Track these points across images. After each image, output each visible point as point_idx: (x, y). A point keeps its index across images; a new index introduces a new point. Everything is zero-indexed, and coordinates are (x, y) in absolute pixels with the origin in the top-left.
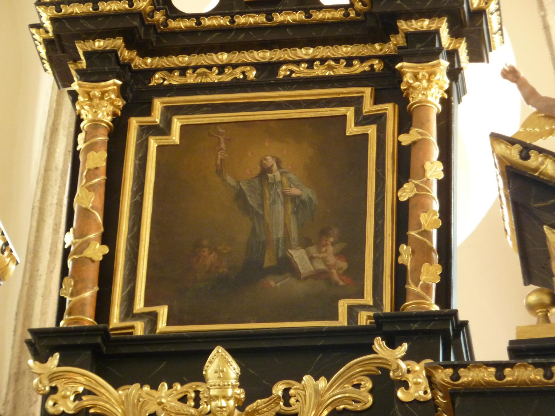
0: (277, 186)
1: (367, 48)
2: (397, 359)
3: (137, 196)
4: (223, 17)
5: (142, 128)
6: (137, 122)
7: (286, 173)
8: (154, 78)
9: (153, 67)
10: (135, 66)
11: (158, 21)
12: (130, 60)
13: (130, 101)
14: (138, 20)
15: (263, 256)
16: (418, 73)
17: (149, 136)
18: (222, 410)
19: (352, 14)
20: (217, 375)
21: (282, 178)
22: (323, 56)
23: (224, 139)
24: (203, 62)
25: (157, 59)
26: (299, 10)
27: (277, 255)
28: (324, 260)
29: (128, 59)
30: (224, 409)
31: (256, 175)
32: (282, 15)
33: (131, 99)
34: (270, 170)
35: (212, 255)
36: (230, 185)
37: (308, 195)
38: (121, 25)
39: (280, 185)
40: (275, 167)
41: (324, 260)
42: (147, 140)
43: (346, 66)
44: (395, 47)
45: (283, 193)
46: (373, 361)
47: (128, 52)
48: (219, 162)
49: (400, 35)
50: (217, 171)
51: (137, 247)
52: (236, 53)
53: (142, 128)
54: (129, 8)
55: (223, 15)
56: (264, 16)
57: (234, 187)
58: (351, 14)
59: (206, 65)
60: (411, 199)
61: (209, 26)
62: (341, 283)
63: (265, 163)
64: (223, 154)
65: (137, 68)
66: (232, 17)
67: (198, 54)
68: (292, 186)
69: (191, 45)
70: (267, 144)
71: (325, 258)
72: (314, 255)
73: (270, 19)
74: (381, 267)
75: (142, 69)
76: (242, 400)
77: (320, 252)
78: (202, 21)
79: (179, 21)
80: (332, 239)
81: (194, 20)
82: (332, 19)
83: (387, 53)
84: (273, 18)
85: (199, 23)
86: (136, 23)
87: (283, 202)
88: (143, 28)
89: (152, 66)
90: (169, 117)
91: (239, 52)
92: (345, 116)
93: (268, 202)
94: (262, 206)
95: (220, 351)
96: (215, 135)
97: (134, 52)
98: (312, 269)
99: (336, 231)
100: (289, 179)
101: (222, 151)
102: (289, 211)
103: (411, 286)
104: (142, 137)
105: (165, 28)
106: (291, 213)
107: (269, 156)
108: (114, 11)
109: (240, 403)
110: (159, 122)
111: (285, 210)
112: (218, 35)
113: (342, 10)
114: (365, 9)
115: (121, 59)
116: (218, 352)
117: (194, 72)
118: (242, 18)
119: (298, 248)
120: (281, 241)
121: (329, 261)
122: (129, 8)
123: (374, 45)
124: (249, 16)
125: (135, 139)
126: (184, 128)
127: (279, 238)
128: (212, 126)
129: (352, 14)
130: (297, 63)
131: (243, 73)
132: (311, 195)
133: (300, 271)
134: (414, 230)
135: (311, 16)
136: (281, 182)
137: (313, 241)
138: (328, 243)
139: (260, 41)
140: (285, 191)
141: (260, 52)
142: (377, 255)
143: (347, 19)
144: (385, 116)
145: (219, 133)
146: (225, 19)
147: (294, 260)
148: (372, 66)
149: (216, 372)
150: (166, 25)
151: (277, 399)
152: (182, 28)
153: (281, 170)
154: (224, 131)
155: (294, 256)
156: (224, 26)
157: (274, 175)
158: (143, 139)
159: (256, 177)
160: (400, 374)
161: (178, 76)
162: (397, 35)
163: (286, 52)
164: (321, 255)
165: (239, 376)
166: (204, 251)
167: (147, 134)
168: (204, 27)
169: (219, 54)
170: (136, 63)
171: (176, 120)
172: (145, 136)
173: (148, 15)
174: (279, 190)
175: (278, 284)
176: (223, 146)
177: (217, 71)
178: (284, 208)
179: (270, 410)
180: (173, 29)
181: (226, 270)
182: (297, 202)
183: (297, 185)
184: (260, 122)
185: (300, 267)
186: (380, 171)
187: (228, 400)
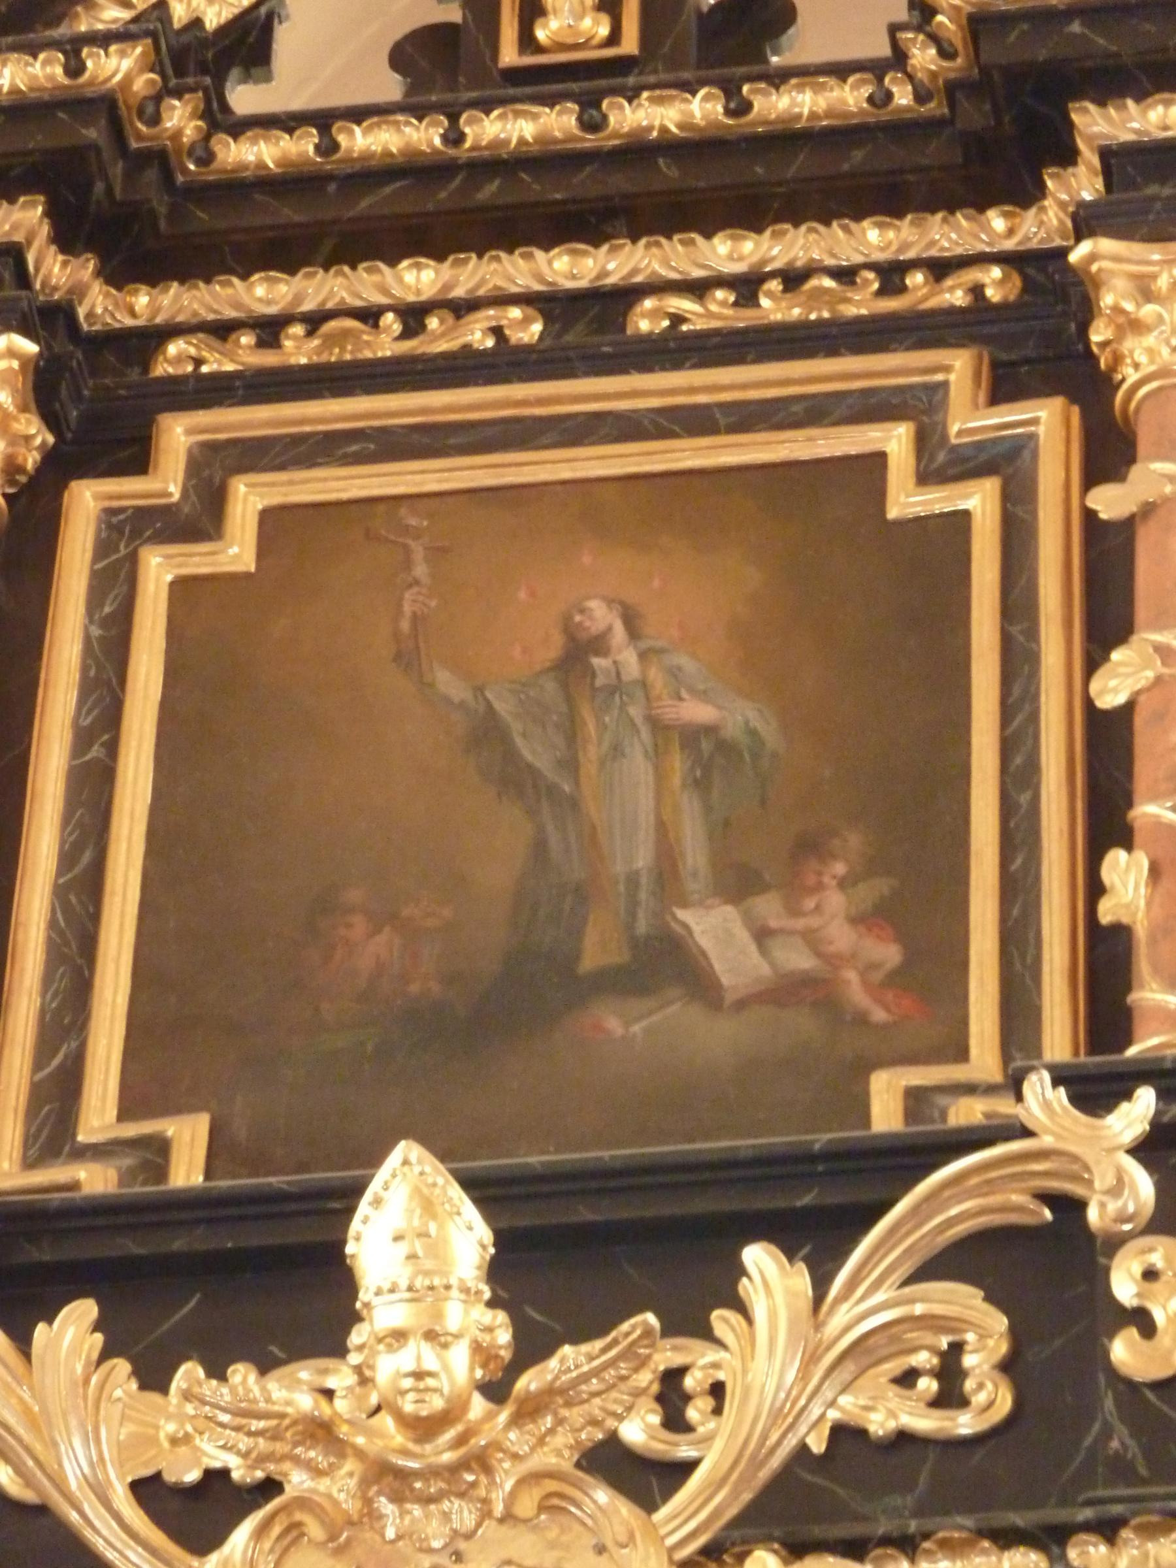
0: (628, 695)
1: (958, 228)
2: (1112, 1150)
3: (96, 747)
4: (420, 119)
5: (114, 520)
6: (97, 497)
7: (661, 651)
8: (161, 358)
9: (158, 320)
10: (90, 315)
11: (177, 134)
12: (70, 291)
13: (69, 435)
14: (103, 122)
15: (577, 933)
16: (1154, 277)
17: (141, 545)
18: (422, 1385)
19: (903, 97)
20: (403, 1248)
21: (644, 672)
22: (795, 259)
23: (425, 549)
24: (345, 295)
25: (172, 291)
26: (703, 83)
27: (630, 926)
28: (812, 939)
29: (65, 289)
30: (430, 1382)
31: (548, 664)
32: (640, 105)
33: (73, 425)
34: (599, 644)
35: (382, 938)
36: (447, 700)
37: (747, 723)
38: (37, 140)
39: (639, 693)
40: (619, 633)
41: (812, 939)
42: (133, 560)
43: (881, 292)
44: (1062, 215)
45: (657, 725)
46: (1018, 1168)
47: (65, 264)
48: (405, 625)
49: (1081, 169)
50: (398, 657)
51: (93, 917)
52: (469, 259)
53: (114, 520)
54: (66, 81)
55: (420, 113)
56: (571, 111)
57: (462, 705)
58: (896, 96)
59: (360, 308)
60: (1142, 699)
61: (367, 156)
62: (879, 1015)
63: (580, 623)
64: (421, 598)
65: (97, 327)
66: (454, 118)
67: (326, 269)
68: (684, 694)
69: (299, 225)
70: (587, 559)
71: (817, 930)
72: (773, 924)
73: (592, 125)
74: (1031, 951)
75: (116, 330)
76: (502, 1353)
77: (795, 912)
78: (342, 139)
79: (254, 141)
80: (840, 868)
81: (313, 136)
82: (829, 114)
83: (1034, 244)
84: (605, 117)
85: (328, 147)
86: (91, 134)
87: (650, 749)
88: (120, 164)
89: (154, 317)
90: (217, 480)
91: (480, 256)
92: (880, 458)
93: (591, 754)
94: (571, 765)
95: (413, 1157)
96: (392, 537)
97: (88, 260)
98: (765, 970)
99: (854, 840)
100: (674, 673)
101: (415, 589)
102: (676, 780)
103: (1152, 990)
104: (117, 550)
105: (203, 170)
106: (684, 786)
107: (595, 597)
108: (10, 92)
109: (492, 1366)
110: (176, 497)
111: (660, 777)
112: (401, 187)
113: (864, 82)
114: (949, 69)
115: (38, 286)
116: (406, 1162)
117: (310, 333)
118: (491, 122)
119: (709, 902)
120: (644, 880)
121: (831, 943)
122: (66, 81)
123: (983, 218)
124: (518, 114)
125: (89, 555)
126: (271, 519)
127: (637, 872)
128: (381, 508)
129: (903, 97)
130: (698, 289)
131: (497, 331)
132: (757, 723)
133: (718, 980)
134: (1155, 797)
135: (746, 107)
136: (644, 684)
137: (767, 877)
138: (826, 879)
139: (556, 203)
140: (659, 711)
141: (560, 255)
142: (1015, 912)
143: (884, 115)
144: (1032, 445)
145: (406, 530)
146: (427, 128)
147: (696, 943)
148: (977, 291)
149: (398, 1238)
150: (207, 158)
151: (640, 1337)
152: (266, 167)
153: (644, 645)
154: (425, 523)
155: (697, 929)
156: (423, 153)
157: (615, 662)
158: (114, 557)
159: (550, 669)
160: (1131, 1208)
161: (250, 347)
162: (1070, 170)
163: (654, 250)
164: (800, 923)
165: (488, 1258)
166: (349, 926)
167: (131, 539)
168: (349, 160)
169: (405, 263)
170: (93, 306)
171: (242, 489)
172: (126, 547)
173: (141, 113)
174: (635, 712)
175: (636, 1028)
176: (421, 570)
177: (397, 328)
178: (656, 768)
179: (612, 1387)
180: (233, 171)
181: (435, 987)
182: (706, 746)
183: (705, 692)
184: (559, 488)
185: (718, 967)
186: (1019, 628)
187: (445, 1346)
